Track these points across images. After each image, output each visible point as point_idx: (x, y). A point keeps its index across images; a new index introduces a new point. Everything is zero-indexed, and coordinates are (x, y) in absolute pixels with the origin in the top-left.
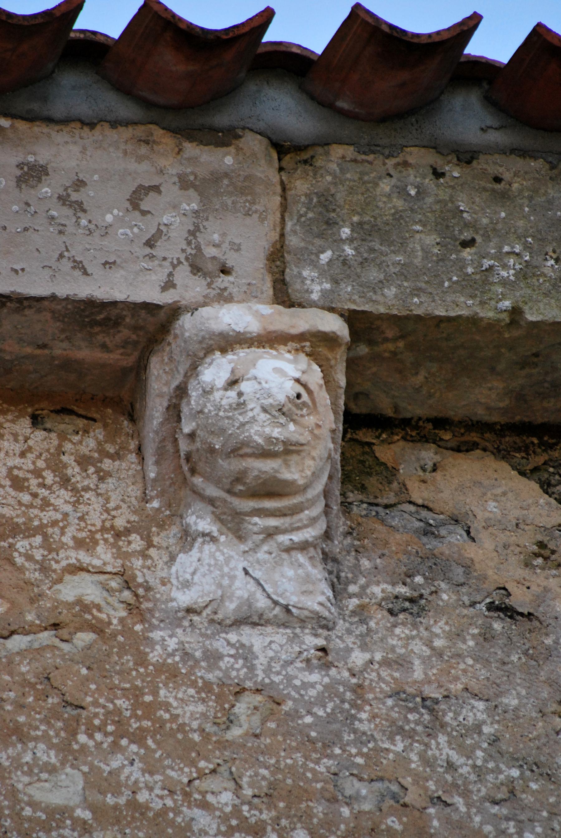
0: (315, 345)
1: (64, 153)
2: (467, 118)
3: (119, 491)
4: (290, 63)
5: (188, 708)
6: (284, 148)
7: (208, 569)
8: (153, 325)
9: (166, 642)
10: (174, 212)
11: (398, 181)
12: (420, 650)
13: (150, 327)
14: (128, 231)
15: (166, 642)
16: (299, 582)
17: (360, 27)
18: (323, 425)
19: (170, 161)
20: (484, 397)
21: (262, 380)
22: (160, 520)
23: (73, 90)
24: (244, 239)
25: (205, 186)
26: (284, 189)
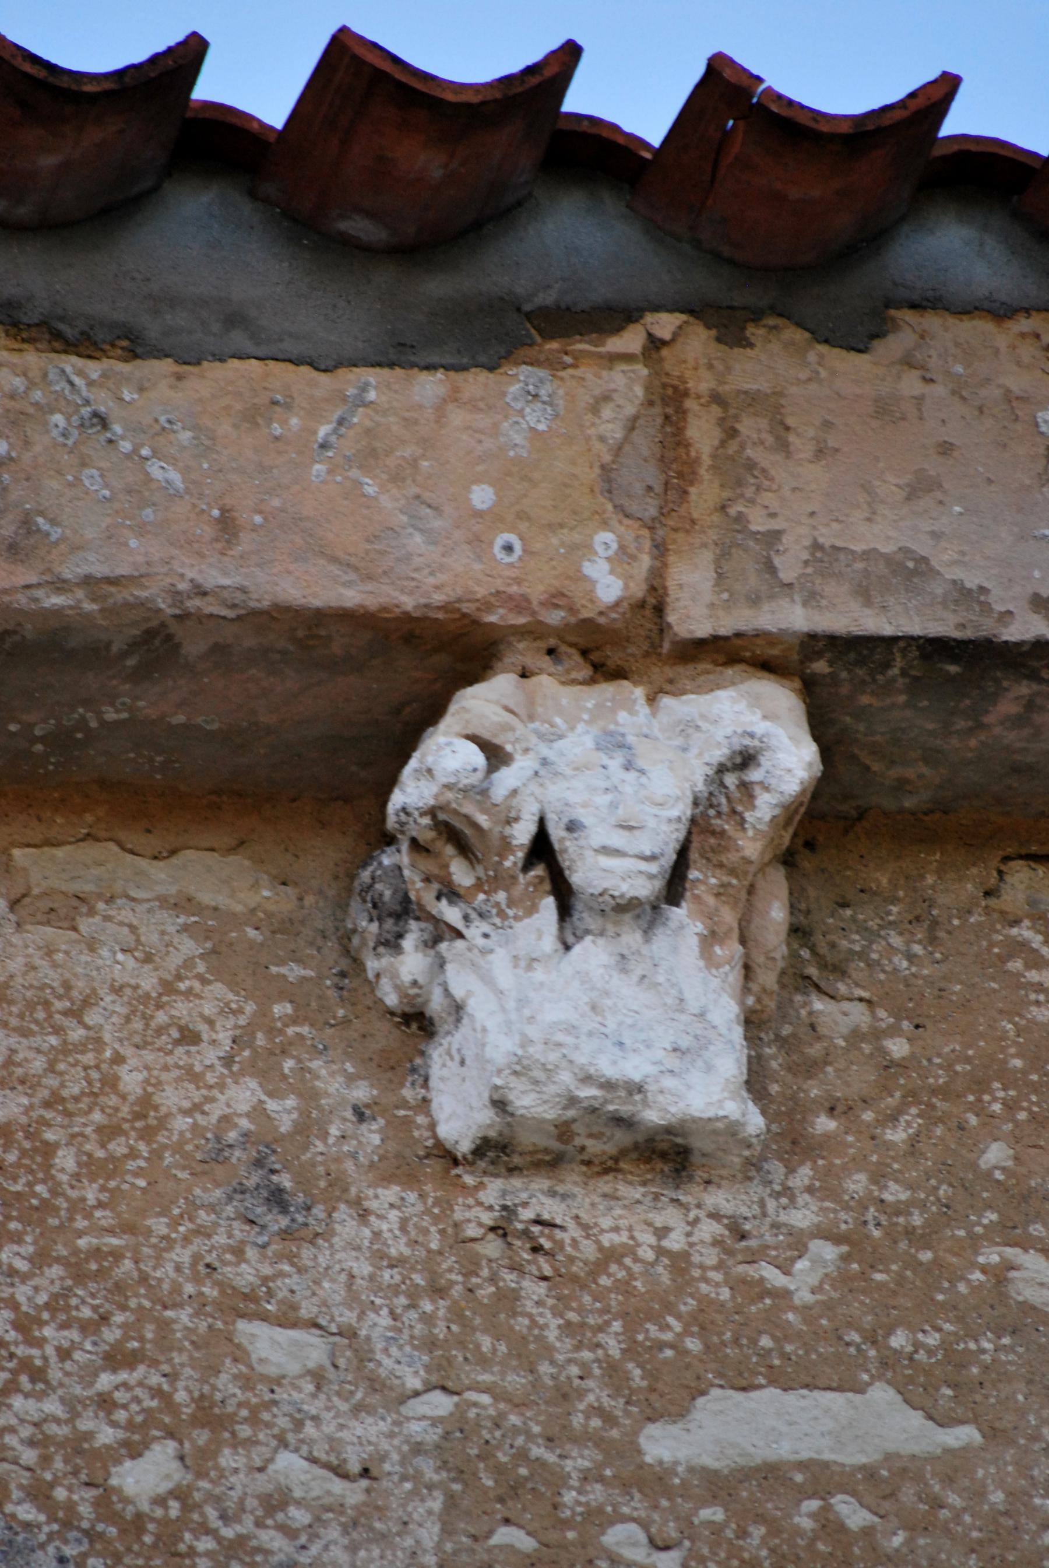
17: (354, 76)
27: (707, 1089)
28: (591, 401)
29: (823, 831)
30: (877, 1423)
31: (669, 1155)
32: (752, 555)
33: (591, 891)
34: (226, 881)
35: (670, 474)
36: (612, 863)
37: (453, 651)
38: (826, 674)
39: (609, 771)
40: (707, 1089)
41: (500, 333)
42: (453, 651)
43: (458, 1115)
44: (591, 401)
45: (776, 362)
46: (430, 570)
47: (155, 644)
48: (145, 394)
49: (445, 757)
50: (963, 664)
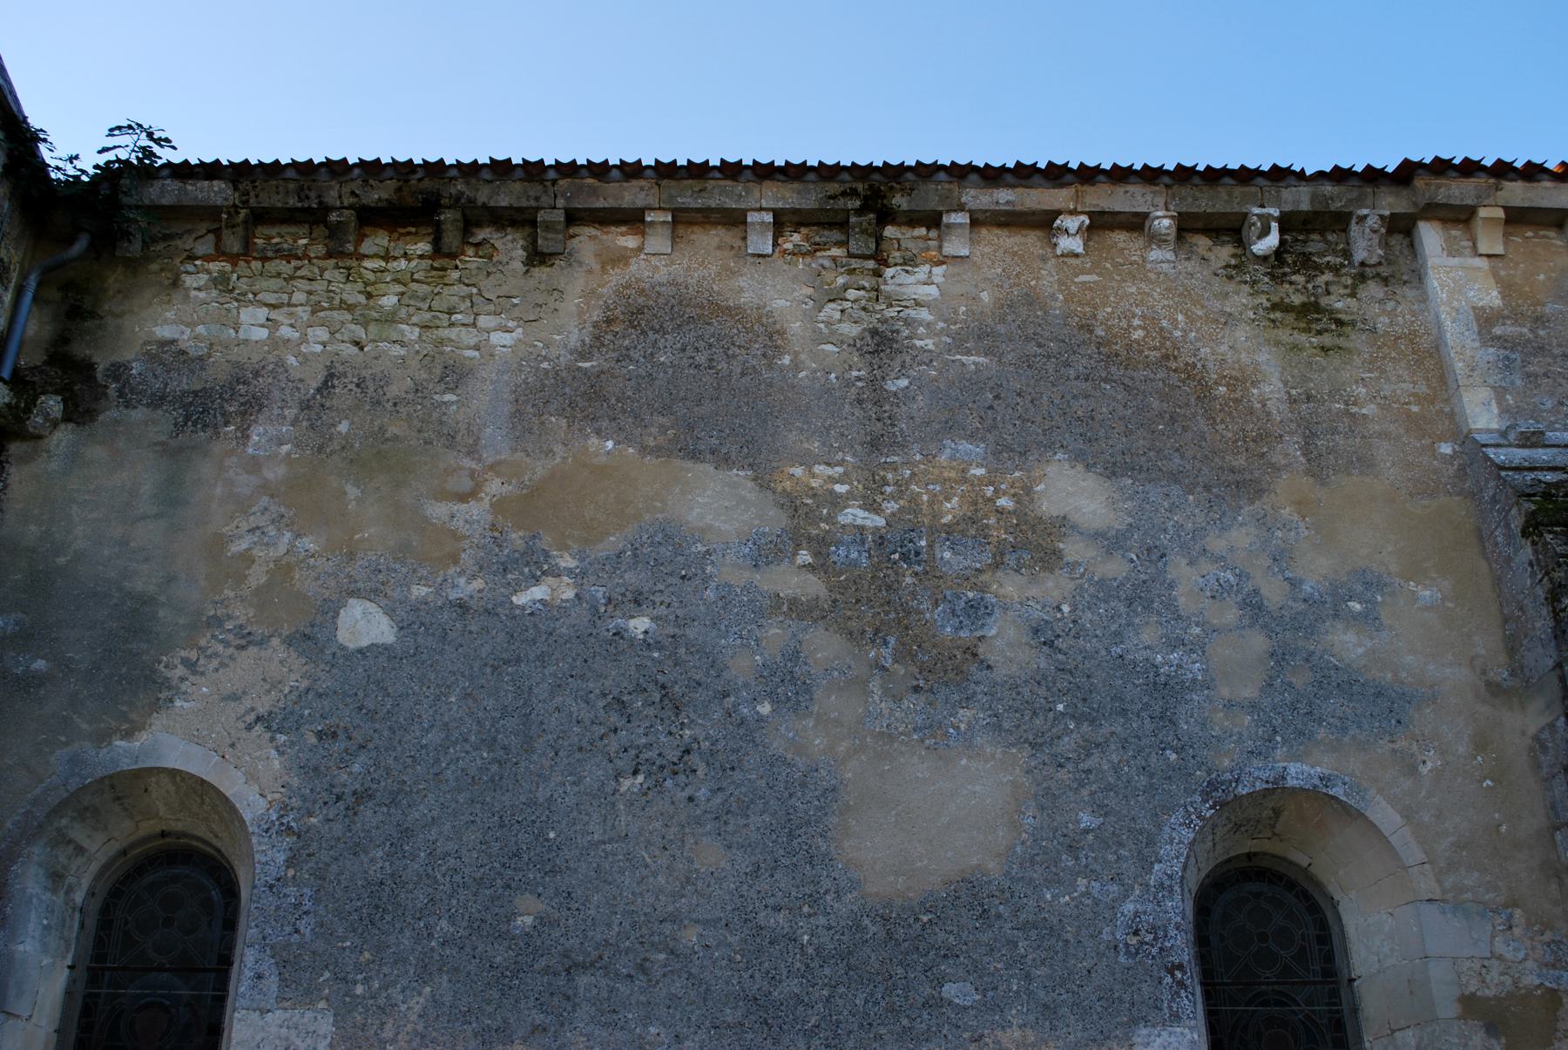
0: (1172, 217)
1: (1131, 188)
2: (1196, 180)
3: (1140, 242)
4: (1168, 172)
5: (1152, 276)
6: (1167, 186)
7: (1155, 254)
8: (1146, 216)
9: (1149, 266)
10: (1149, 197)
11: (1185, 191)
12: (1189, 266)
13: (1145, 216)
14: (1142, 200)
15: (1149, 266)
16: (1170, 256)
17: (1050, 164)
18: (1174, 229)
19: (1148, 189)
20: (1200, 225)
21: (1164, 223)
22: (1147, 247)
23: (1132, 179)
24: (1160, 201)
25: (1154, 193)
26: (1529, 495)
27: (1080, 250)
28: (242, 263)
29: (1090, 228)
30: (1095, 278)
31: (1077, 255)
32: (1084, 204)
33: (642, 183)
34: (1039, 233)
35: (1077, 198)
36: (1072, 231)
37: (1058, 213)
38: (1090, 214)
39: (1072, 223)
40: (1080, 250)
41: (1062, 186)
42: (1058, 213)
43: (1059, 252)
44: (242, 263)
45: (1085, 188)
46: (1057, 206)
47: (1033, 213)
48: (1033, 192)
49: (1058, 222)
50: (1102, 213)
